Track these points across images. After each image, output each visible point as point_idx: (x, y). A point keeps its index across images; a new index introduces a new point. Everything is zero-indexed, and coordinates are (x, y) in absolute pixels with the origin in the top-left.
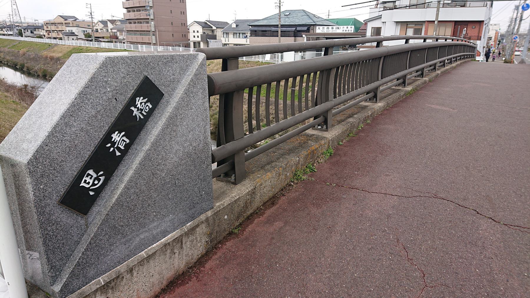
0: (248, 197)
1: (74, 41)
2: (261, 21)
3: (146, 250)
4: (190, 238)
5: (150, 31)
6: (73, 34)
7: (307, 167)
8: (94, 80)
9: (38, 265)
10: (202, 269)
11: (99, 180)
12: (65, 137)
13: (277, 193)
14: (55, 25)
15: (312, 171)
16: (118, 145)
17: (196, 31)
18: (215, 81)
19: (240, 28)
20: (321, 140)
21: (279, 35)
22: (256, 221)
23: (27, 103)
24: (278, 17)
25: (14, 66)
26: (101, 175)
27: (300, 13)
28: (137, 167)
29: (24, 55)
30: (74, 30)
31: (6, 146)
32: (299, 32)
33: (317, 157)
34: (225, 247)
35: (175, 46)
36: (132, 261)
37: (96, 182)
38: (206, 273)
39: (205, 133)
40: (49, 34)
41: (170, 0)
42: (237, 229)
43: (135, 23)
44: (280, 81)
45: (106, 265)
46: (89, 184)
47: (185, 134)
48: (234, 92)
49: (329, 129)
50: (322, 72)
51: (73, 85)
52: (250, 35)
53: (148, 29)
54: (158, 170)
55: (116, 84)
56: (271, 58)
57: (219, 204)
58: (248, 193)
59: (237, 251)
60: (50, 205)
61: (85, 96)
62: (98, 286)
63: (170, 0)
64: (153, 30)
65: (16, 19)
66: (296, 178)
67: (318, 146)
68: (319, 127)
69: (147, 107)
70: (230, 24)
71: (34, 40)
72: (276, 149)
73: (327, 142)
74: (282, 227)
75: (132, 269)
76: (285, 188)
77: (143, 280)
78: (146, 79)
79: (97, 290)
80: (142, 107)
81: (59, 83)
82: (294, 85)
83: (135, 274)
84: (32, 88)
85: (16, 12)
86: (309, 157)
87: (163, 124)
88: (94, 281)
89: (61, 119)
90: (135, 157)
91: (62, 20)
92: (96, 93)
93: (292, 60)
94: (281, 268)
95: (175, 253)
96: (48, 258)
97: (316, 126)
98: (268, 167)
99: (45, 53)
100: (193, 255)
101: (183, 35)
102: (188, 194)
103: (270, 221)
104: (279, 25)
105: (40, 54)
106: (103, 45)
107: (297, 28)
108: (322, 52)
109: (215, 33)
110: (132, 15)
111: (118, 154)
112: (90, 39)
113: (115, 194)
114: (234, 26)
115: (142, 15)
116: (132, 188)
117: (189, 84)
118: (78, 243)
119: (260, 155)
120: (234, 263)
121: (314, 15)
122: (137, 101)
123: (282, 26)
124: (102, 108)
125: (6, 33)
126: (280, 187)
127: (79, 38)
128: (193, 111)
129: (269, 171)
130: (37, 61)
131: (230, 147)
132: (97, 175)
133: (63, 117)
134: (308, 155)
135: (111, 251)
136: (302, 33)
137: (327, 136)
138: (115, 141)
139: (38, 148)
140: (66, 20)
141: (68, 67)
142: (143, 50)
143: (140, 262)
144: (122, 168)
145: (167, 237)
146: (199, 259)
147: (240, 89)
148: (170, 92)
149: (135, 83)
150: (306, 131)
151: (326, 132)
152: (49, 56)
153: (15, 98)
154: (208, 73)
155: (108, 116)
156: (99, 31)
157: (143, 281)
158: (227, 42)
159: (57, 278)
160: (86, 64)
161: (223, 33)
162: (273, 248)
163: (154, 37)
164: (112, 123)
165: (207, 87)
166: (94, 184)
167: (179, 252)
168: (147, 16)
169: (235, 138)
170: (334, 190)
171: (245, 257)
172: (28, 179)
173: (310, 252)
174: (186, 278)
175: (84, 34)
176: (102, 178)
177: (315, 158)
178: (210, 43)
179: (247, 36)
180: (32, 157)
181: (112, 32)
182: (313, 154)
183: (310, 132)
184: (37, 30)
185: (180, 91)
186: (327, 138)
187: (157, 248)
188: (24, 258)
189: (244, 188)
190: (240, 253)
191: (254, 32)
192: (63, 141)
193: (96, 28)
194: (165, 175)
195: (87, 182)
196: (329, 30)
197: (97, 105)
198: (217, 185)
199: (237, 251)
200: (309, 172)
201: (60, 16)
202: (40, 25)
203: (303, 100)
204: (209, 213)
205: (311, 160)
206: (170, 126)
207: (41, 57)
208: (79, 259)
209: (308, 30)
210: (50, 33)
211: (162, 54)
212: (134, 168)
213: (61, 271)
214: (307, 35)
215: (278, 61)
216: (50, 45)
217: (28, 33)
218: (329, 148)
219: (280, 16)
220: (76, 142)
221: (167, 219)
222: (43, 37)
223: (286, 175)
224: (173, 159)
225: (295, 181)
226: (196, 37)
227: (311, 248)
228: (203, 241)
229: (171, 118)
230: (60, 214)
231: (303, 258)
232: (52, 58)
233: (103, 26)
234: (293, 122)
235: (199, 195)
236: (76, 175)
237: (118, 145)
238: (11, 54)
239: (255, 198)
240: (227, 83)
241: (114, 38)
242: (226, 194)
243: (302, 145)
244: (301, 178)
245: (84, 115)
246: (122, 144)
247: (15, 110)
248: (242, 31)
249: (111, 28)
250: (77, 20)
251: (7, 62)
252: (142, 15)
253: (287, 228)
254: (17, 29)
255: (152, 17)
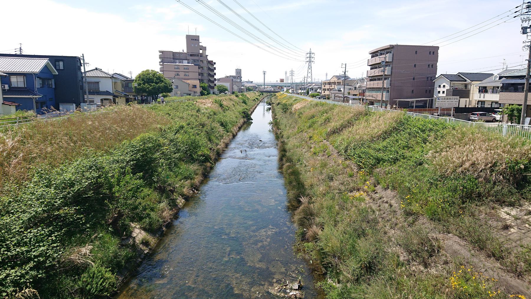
110: (377, 72)
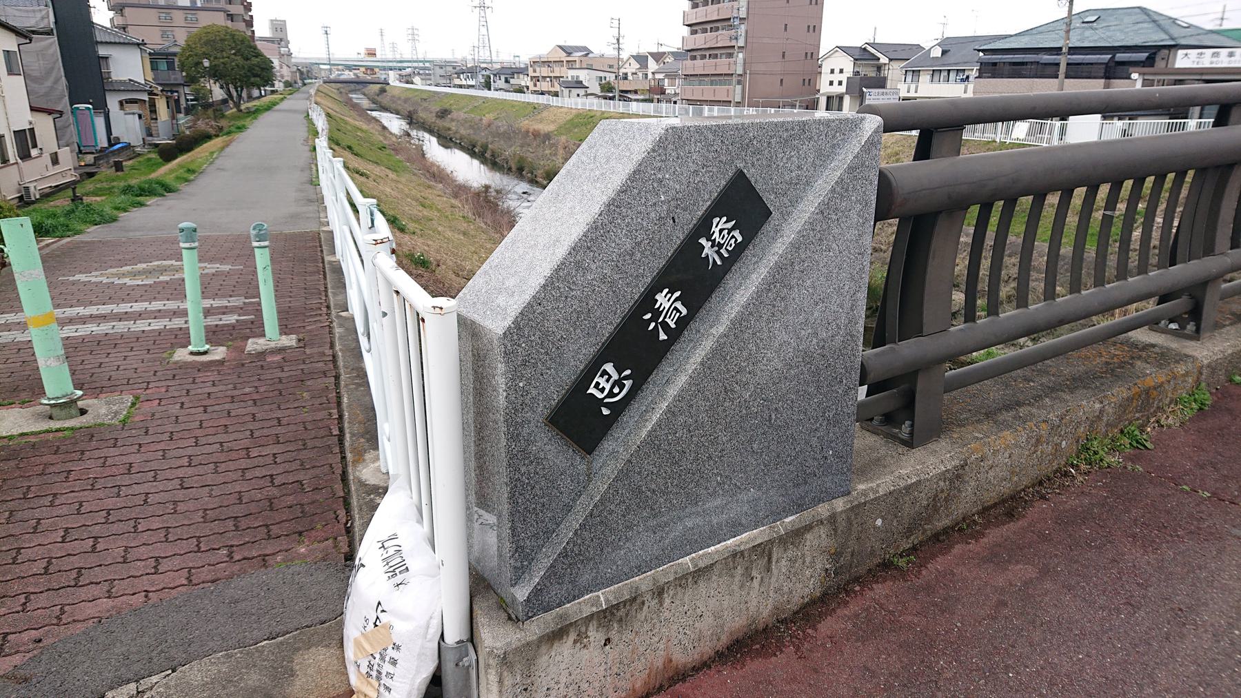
0: (942, 483)
1: (579, 100)
2: (1012, 39)
3: (694, 555)
4: (790, 553)
5: (732, 74)
6: (579, 84)
7: (1122, 432)
8: (638, 177)
9: (492, 539)
10: (810, 631)
11: (622, 387)
12: (572, 290)
13: (1024, 490)
14: (549, 66)
15: (1139, 446)
16: (665, 317)
17: (837, 71)
18: (895, 184)
19: (950, 58)
20: (1175, 362)
21: (1060, 73)
22: (957, 549)
23: (485, 220)
24: (1064, 27)
25: (470, 148)
26: (626, 378)
27: (1130, 14)
28: (696, 369)
29: (489, 126)
30: (583, 76)
31: (468, 297)
32: (1121, 67)
33: (1158, 408)
34: (869, 594)
35: (784, 106)
36: (664, 573)
37: (616, 390)
38: (819, 643)
39: (853, 310)
40: (535, 85)
41: (788, 2)
42: (904, 559)
43: (703, 57)
44: (1046, 195)
45: (614, 568)
46: (603, 393)
47: (806, 309)
48: (941, 212)
49: (1205, 335)
50: (1202, 171)
51: (598, 185)
52: (977, 75)
53: (729, 69)
54: (737, 383)
55: (678, 187)
56: (1028, 134)
57: (864, 487)
58: (943, 473)
59: (900, 611)
60: (530, 422)
61: (618, 210)
62: (594, 609)
63: (788, 2)
64: (740, 71)
65: (484, 55)
66: (1085, 459)
67: (1163, 379)
68: (1173, 326)
69: (733, 241)
70: (927, 49)
71: (510, 96)
72: (1033, 370)
73: (1195, 370)
74: (1031, 580)
75: (663, 589)
76: (1049, 480)
77: (682, 621)
78: (740, 175)
79: (590, 618)
80: (723, 239)
81: (572, 181)
82: (1111, 203)
83: (667, 601)
84: (498, 192)
85: (486, 42)
86: (1134, 405)
87: (760, 280)
88: (588, 596)
89: (570, 253)
90: (694, 348)
91: (562, 56)
92: (639, 205)
93: (1093, 138)
94: (1021, 684)
95: (752, 579)
96: (513, 529)
97: (1163, 322)
98: (1007, 416)
99: (525, 124)
100: (791, 593)
101: (804, 80)
102: (795, 449)
103: (996, 558)
104: (1064, 49)
105: (517, 126)
106: (634, 107)
107: (1118, 55)
108: (1186, 118)
109: (885, 73)
110: (700, 40)
111: (663, 336)
112: (611, 95)
113: (647, 420)
114: (937, 52)
115: (721, 38)
116: (681, 414)
117: (833, 190)
118: (568, 509)
119: (986, 382)
120: (893, 639)
121: (1174, 21)
122: (714, 226)
123: (1073, 50)
124: (646, 237)
125: (464, 82)
126: (1034, 473)
127: (589, 91)
128: (831, 254)
129: (1009, 427)
130: (510, 139)
131: (907, 350)
132: (620, 375)
133: (574, 250)
134: (1133, 399)
135: (627, 540)
136: (1131, 69)
137: (1195, 354)
138: (661, 309)
139: (525, 307)
140: (569, 54)
141: (590, 148)
142: (732, 116)
143: (680, 579)
144: (665, 368)
145: (738, 537)
146: (804, 607)
147: (954, 206)
148: (786, 208)
149: (715, 185)
150: (1130, 334)
151: (1193, 343)
152: (531, 130)
153: (467, 210)
154: (883, 165)
155: (654, 255)
156: (630, 77)
157: (680, 622)
158: (912, 94)
159: (523, 573)
160: (627, 142)
161: (906, 71)
162: (1003, 628)
163: (739, 88)
164: (660, 271)
165: (874, 198)
166: (611, 394)
167: (762, 578)
168: (731, 41)
169: (1216, 247)
170: (1204, 508)
171: (921, 631)
172: (500, 365)
173: (1112, 664)
174: (772, 643)
175: (600, 84)
176: (628, 383)
177: (1152, 410)
178: (868, 97)
179: (968, 77)
180: (513, 323)
181: (654, 79)
182: (1146, 400)
183: (1142, 336)
184: (516, 75)
185: (808, 207)
186: (1194, 359)
187: (716, 558)
188: (469, 518)
189: (932, 459)
190: (910, 618)
191: (991, 67)
192: (569, 299)
193: (625, 71)
194: (750, 396)
195: (600, 387)
196: (1220, 59)
197: (637, 231)
198: (865, 441)
199: (901, 613)
200: (1128, 446)
201: (560, 47)
202: (522, 66)
203: (1114, 247)
204: (840, 504)
205: (1137, 415)
206: (775, 287)
207: (516, 132)
208: (567, 543)
209: (1150, 62)
210: (538, 83)
211: (782, 120)
212: (690, 372)
213: (533, 559)
214: (1144, 74)
215: (1049, 140)
216: (535, 108)
217: (501, 83)
218: (1197, 388)
219: (1069, 24)
220: (591, 303)
221: (743, 497)
222: (525, 90)
223: (1056, 444)
224: (772, 362)
225: (1083, 467)
226: (836, 83)
227: (1115, 654)
228: (819, 566)
229: (779, 267)
230: (545, 445)
231: (1087, 674)
232: (536, 134)
233: (638, 66)
234: (1096, 304)
235: (819, 457)
236: (583, 371)
237: (665, 317)
238: (469, 124)
239: (959, 491)
240: (924, 190)
241: (656, 93)
242: (885, 467)
243: (1115, 372)
244: (1101, 460)
245: (611, 250)
246: (672, 317)
247: (464, 234)
248: (956, 64)
249: (653, 71)
250: (590, 55)
251: (461, 139)
252: (721, 38)
253: (1048, 585)
254: (483, 75)
255: (741, 43)
